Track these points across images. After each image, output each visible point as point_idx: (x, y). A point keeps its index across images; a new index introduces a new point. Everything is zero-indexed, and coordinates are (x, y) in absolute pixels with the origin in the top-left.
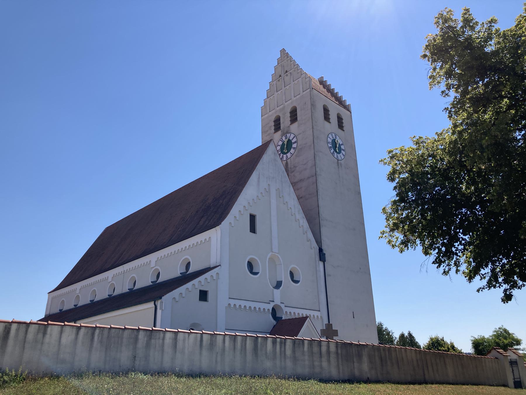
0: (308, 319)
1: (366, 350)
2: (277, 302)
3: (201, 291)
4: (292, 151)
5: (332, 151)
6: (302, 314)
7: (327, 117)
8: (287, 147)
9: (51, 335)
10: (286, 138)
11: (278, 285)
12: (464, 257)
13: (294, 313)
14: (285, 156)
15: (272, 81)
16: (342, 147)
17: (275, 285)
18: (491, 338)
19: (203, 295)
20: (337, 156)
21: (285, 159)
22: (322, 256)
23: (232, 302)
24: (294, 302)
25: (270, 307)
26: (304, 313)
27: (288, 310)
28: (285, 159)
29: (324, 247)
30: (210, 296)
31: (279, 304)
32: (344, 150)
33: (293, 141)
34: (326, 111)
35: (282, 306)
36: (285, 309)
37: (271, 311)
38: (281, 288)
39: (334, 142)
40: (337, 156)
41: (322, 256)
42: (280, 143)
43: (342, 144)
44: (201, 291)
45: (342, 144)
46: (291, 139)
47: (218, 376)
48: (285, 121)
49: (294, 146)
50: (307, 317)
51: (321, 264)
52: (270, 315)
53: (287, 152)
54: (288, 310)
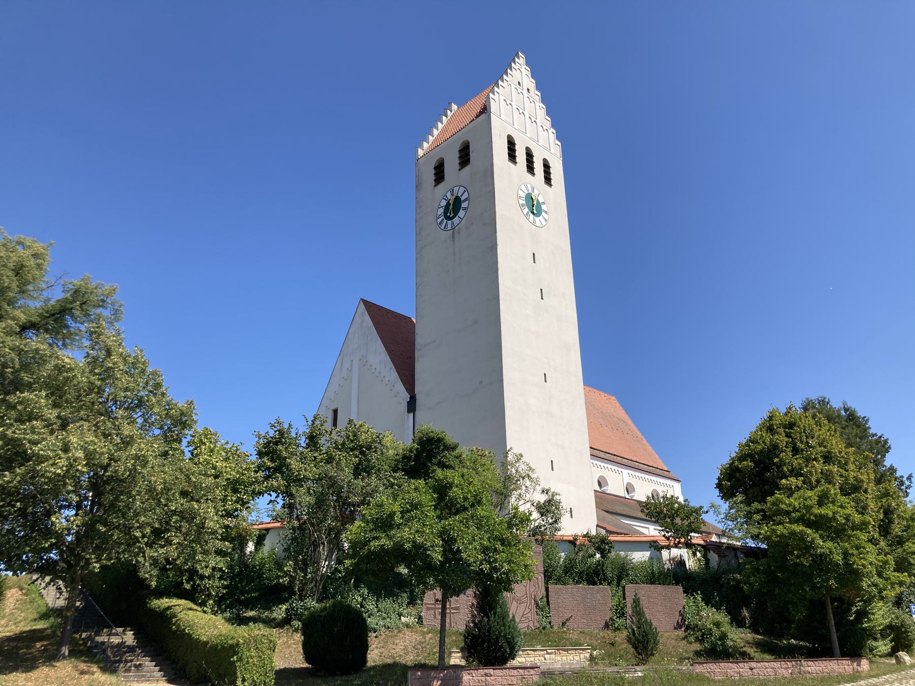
4: (461, 213)
5: (526, 210)
8: (453, 209)
9: (190, 609)
10: (452, 195)
12: (324, 449)
14: (450, 222)
16: (544, 207)
18: (525, 501)
20: (534, 220)
21: (449, 227)
28: (449, 227)
32: (546, 212)
33: (462, 199)
39: (530, 199)
40: (534, 220)
42: (444, 203)
43: (544, 203)
45: (544, 203)
46: (459, 195)
47: (188, 679)
49: (464, 205)
53: (454, 217)
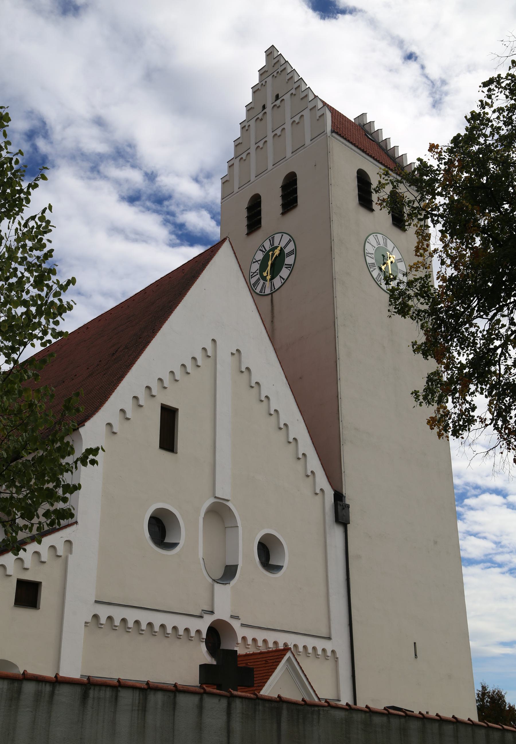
0: (289, 655)
1: (436, 256)
2: (222, 613)
3: (20, 582)
6: (275, 643)
7: (365, 200)
8: (272, 265)
11: (230, 572)
13: (265, 641)
15: (248, 120)
17: (219, 573)
19: (28, 594)
22: (341, 514)
23: (104, 612)
24: (256, 608)
25: (204, 625)
26: (282, 639)
27: (250, 634)
29: (348, 491)
30: (46, 596)
31: (226, 617)
34: (363, 179)
35: (235, 624)
36: (240, 632)
37: (204, 636)
38: (233, 582)
41: (341, 514)
42: (260, 256)
44: (20, 582)
48: (272, 204)
50: (286, 649)
51: (338, 532)
52: (203, 647)
54: (250, 634)
